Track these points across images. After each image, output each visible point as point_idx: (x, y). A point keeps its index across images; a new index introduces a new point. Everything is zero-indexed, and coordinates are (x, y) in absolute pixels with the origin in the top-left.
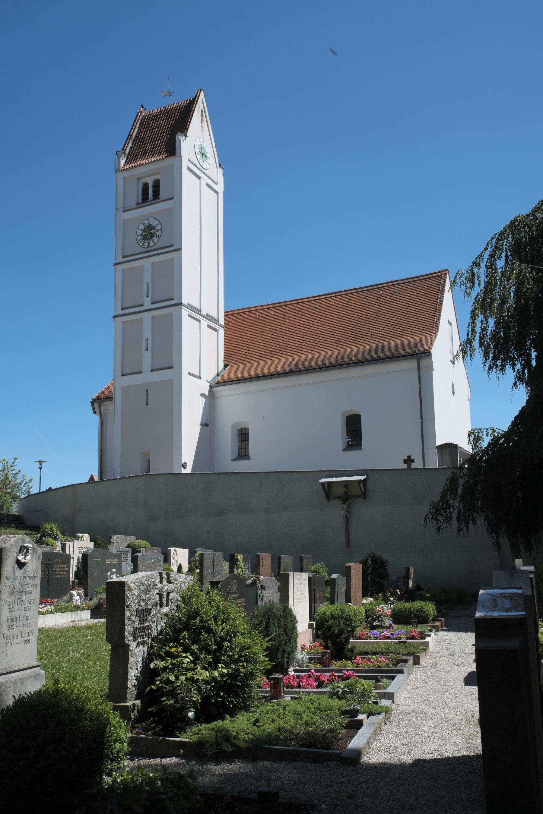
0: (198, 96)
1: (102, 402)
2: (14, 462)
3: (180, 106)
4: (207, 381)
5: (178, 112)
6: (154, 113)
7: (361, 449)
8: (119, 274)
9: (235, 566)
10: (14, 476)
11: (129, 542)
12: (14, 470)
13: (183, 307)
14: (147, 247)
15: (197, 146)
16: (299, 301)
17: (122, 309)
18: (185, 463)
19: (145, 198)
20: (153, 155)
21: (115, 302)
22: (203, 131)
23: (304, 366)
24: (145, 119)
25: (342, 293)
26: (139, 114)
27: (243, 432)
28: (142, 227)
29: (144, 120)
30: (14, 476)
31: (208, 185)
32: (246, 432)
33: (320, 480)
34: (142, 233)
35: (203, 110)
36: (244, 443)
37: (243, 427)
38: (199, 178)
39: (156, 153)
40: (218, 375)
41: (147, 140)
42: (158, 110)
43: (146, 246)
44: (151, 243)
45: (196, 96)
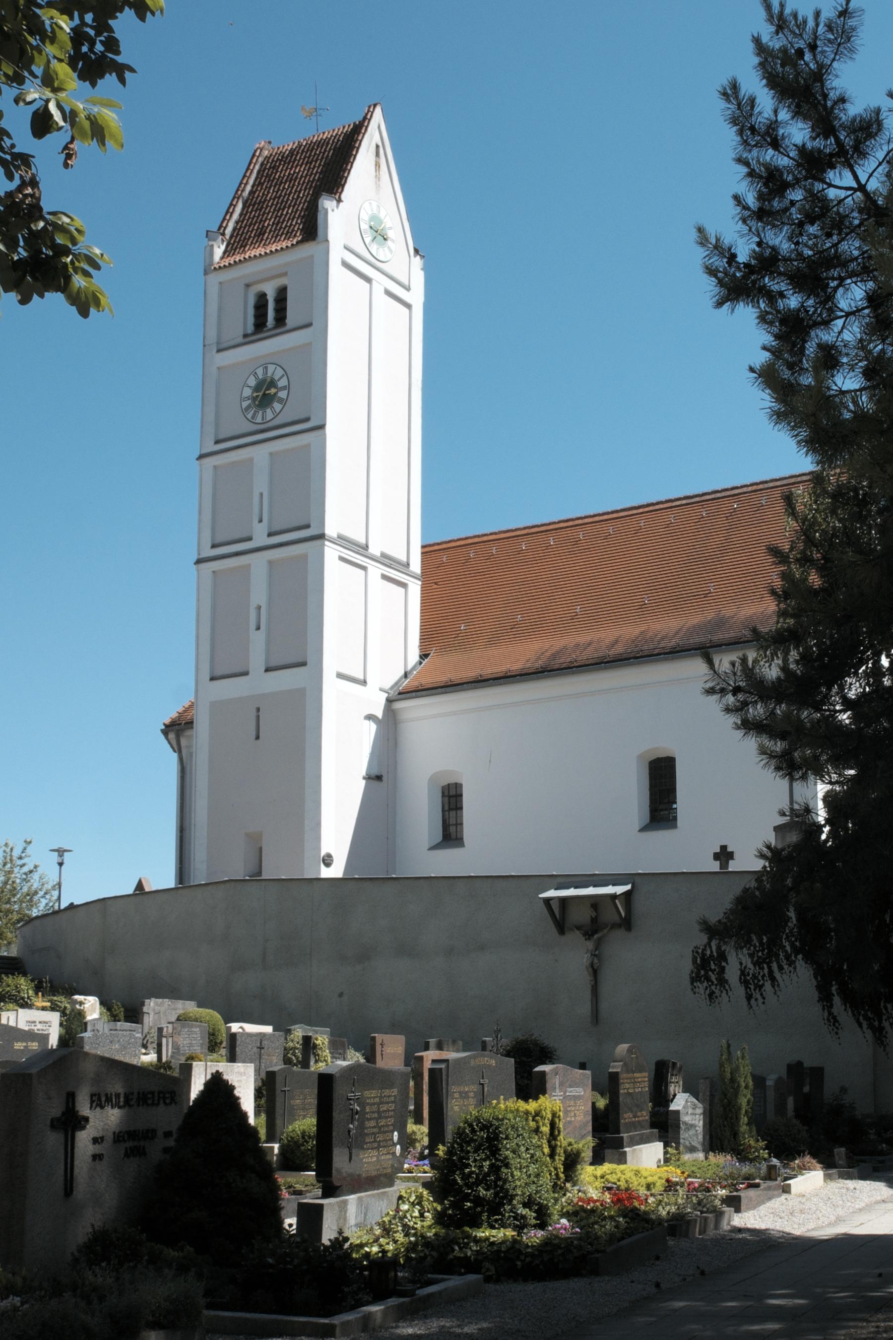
0: (369, 117)
1: (183, 730)
2: (25, 849)
3: (335, 137)
4: (381, 690)
5: (330, 149)
6: (287, 150)
7: (675, 826)
8: (208, 476)
9: (312, 1057)
10: (24, 876)
11: (181, 1012)
12: (24, 865)
13: (327, 543)
14: (261, 422)
15: (365, 216)
16: (586, 521)
17: (214, 546)
18: (329, 856)
19: (260, 324)
20: (276, 238)
21: (199, 533)
22: (378, 187)
23: (568, 660)
24: (268, 162)
25: (661, 506)
26: (257, 154)
27: (453, 793)
28: (252, 382)
29: (266, 165)
30: (24, 876)
31: (388, 293)
32: (458, 793)
33: (540, 893)
34: (253, 393)
35: (380, 144)
36: (453, 813)
37: (452, 780)
38: (368, 280)
39: (282, 234)
40: (406, 675)
41: (267, 206)
42: (294, 143)
43: (259, 419)
44: (269, 414)
45: (365, 118)
